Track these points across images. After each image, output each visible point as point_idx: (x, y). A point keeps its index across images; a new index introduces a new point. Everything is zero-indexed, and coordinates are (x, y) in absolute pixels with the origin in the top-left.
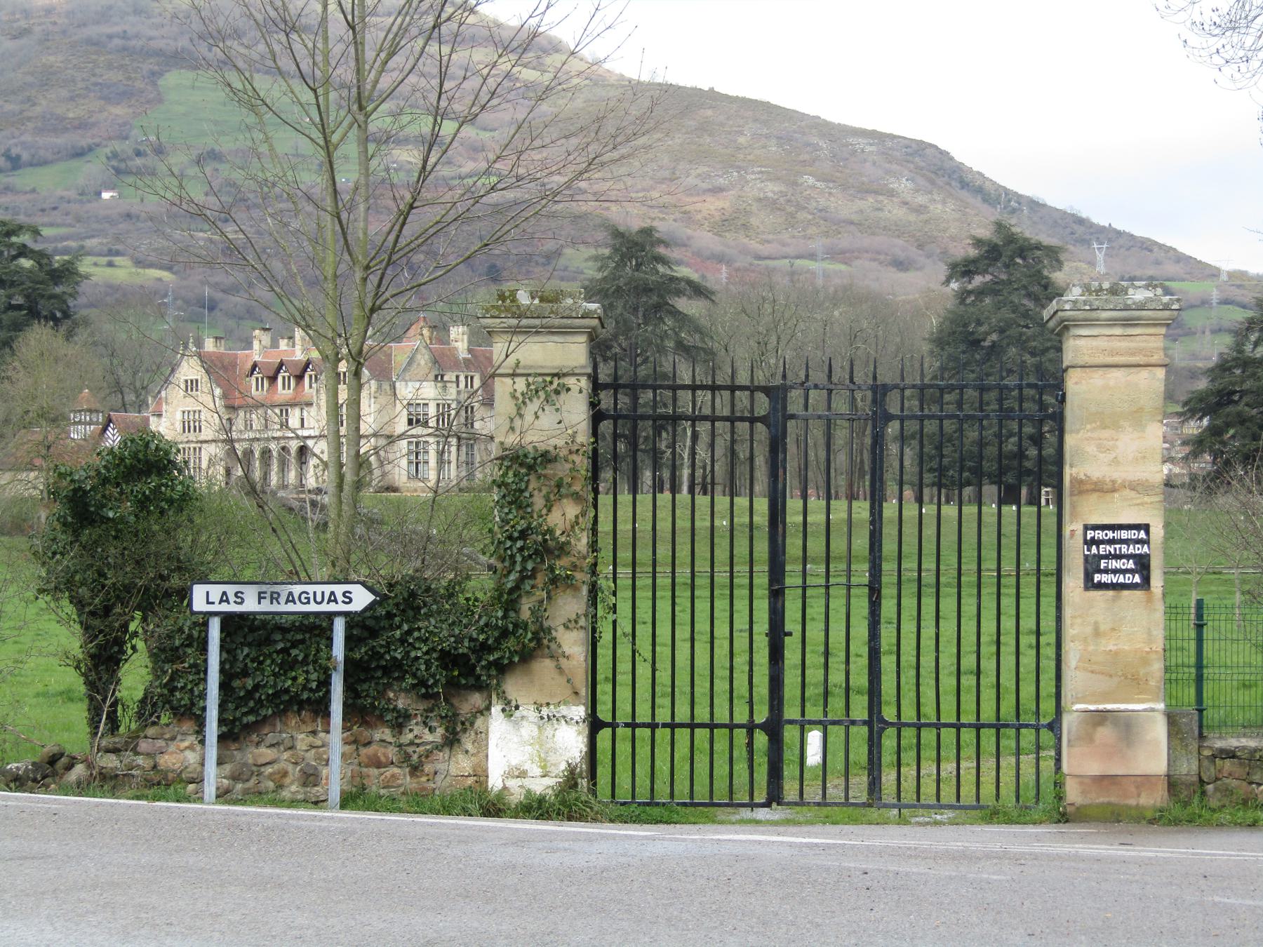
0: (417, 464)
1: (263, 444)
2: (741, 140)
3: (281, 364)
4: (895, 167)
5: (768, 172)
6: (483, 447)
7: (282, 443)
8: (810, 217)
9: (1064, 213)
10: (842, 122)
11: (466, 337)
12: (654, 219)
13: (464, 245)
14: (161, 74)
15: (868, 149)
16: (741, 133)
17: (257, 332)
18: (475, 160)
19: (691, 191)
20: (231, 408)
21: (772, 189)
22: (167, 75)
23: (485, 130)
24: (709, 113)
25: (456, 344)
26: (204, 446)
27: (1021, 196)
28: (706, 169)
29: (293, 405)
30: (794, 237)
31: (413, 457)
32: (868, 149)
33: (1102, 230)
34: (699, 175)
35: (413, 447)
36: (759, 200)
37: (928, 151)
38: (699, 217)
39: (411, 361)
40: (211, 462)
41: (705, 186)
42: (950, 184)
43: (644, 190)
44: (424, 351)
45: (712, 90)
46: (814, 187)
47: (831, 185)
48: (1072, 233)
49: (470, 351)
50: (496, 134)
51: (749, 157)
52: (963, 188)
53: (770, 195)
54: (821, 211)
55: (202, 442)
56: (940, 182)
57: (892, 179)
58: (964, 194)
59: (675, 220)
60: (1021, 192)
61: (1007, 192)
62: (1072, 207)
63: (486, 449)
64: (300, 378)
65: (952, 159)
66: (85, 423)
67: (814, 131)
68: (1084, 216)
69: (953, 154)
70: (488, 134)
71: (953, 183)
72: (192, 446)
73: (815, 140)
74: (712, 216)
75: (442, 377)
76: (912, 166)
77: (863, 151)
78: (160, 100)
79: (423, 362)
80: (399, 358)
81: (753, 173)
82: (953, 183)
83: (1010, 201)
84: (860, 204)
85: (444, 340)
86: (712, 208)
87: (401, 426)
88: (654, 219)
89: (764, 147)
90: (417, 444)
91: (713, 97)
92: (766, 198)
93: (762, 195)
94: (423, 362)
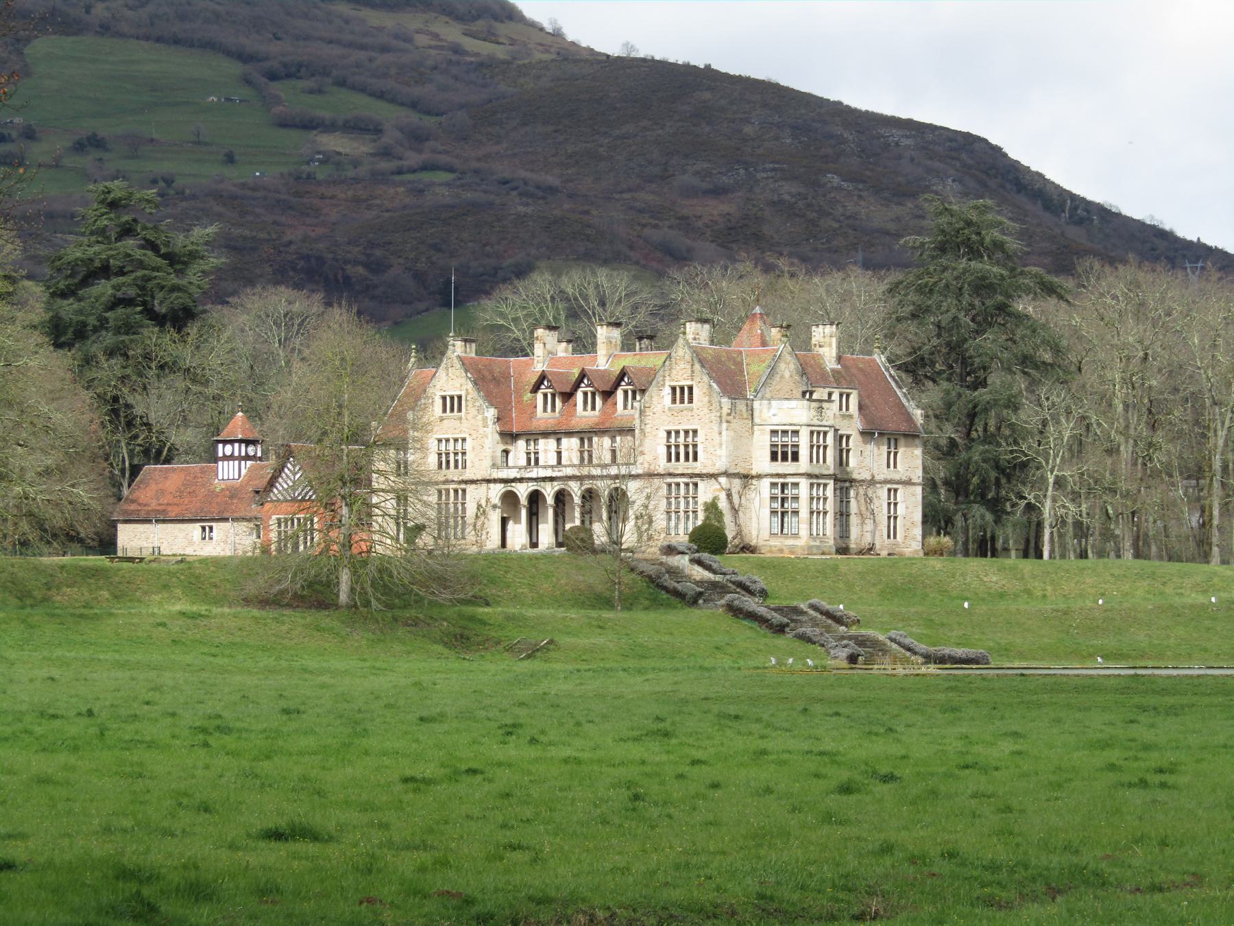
0: (782, 511)
1: (557, 486)
2: (748, 129)
3: (623, 374)
4: (937, 164)
5: (782, 170)
6: (861, 491)
7: (587, 484)
8: (836, 225)
9: (1141, 225)
10: (870, 109)
11: (834, 340)
12: (644, 226)
13: (412, 255)
14: (28, 40)
15: (905, 142)
16: (747, 121)
17: (540, 332)
18: (420, 151)
19: (690, 192)
20: (509, 436)
21: (788, 190)
22: (36, 42)
23: (428, 113)
24: (707, 95)
25: (821, 351)
26: (470, 489)
27: (1090, 203)
28: (706, 165)
29: (602, 432)
30: (816, 250)
31: (777, 505)
32: (905, 142)
33: (1188, 245)
34: (697, 173)
35: (778, 491)
36: (774, 204)
37: (977, 146)
38: (700, 224)
39: (773, 371)
40: (481, 511)
41: (705, 185)
42: (1003, 186)
43: (630, 190)
44: (788, 358)
45: (708, 67)
46: (839, 188)
47: (861, 186)
48: (1153, 249)
49: (839, 359)
50: (443, 119)
51: (760, 151)
52: (1019, 191)
53: (787, 197)
54: (849, 218)
55: (466, 482)
56: (992, 183)
57: (935, 181)
58: (1021, 199)
59: (670, 227)
60: (1089, 198)
61: (1073, 197)
62: (1152, 217)
63: (866, 495)
64: (608, 394)
65: (1005, 155)
66: (240, 458)
67: (838, 119)
68: (1167, 227)
69: (1006, 150)
70: (434, 119)
71: (1008, 186)
72: (681, 480)
73: (838, 130)
74: (716, 223)
75: (811, 393)
76: (958, 164)
77: (897, 144)
78: (26, 72)
79: (787, 374)
80: (754, 368)
81: (764, 170)
82: (1008, 186)
83: (1076, 208)
84: (896, 210)
85: (806, 344)
86: (715, 212)
87: (761, 462)
88: (644, 226)
89: (777, 138)
90: (784, 486)
91: (707, 78)
92: (781, 202)
93: (776, 198)
94: (787, 374)
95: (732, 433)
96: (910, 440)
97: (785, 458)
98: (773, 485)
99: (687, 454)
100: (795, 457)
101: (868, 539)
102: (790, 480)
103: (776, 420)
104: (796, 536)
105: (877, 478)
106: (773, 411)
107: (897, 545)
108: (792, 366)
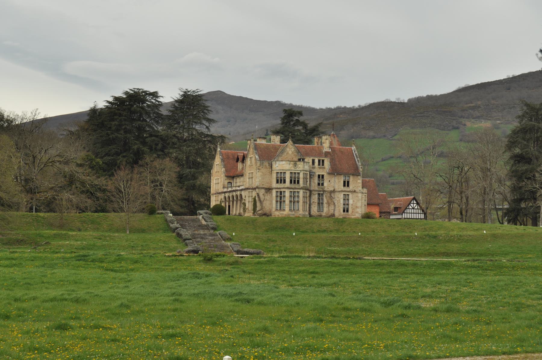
9: (233, 96)
44: (291, 146)
79: (290, 152)
94: (290, 152)
95: (261, 173)
96: (355, 177)
97: (281, 183)
98: (277, 192)
99: (295, 181)
100: (285, 182)
101: (332, 212)
102: (296, 190)
103: (278, 168)
104: (284, 210)
105: (337, 189)
106: (277, 165)
107: (349, 215)
108: (293, 150)
